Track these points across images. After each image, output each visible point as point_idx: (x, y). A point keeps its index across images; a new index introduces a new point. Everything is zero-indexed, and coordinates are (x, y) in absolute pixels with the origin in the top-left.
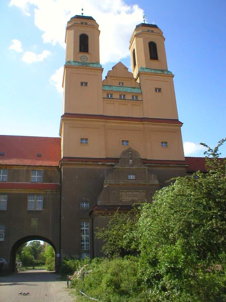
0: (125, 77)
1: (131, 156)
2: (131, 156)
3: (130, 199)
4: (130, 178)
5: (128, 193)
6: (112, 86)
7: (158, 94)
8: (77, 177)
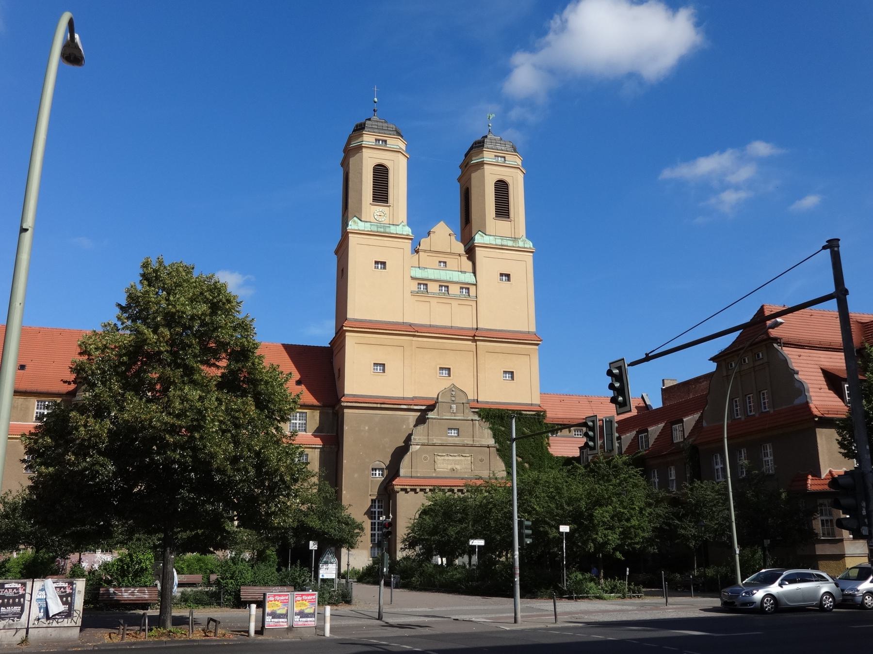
3: (450, 467)
5: (446, 458)
7: (505, 284)
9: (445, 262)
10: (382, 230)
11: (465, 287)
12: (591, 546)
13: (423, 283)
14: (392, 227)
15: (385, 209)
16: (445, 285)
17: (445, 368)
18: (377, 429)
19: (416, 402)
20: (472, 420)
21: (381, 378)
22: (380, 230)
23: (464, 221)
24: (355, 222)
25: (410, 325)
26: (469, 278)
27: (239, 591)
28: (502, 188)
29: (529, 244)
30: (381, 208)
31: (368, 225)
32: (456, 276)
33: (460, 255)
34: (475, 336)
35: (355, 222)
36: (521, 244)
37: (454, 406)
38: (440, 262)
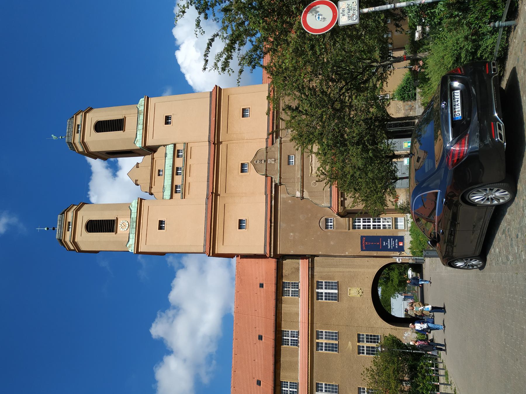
0: (150, 168)
1: (263, 162)
2: (263, 162)
4: (292, 162)
6: (164, 186)
7: (173, 120)
8: (292, 234)
9: (159, 171)
10: (135, 224)
11: (177, 153)
12: (385, 36)
13: (174, 189)
14: (132, 216)
15: (120, 222)
16: (176, 171)
17: (302, 257)
18: (292, 225)
19: (269, 193)
20: (281, 143)
21: (252, 113)
22: (134, 226)
23: (131, 154)
24: (129, 247)
25: (207, 198)
26: (170, 150)
27: (417, 330)
28: (101, 127)
29: (142, 101)
30: (119, 226)
31: (131, 236)
32: (169, 161)
33: (153, 159)
34: (216, 143)
35: (129, 247)
36: (141, 108)
37: (269, 161)
38: (159, 175)
